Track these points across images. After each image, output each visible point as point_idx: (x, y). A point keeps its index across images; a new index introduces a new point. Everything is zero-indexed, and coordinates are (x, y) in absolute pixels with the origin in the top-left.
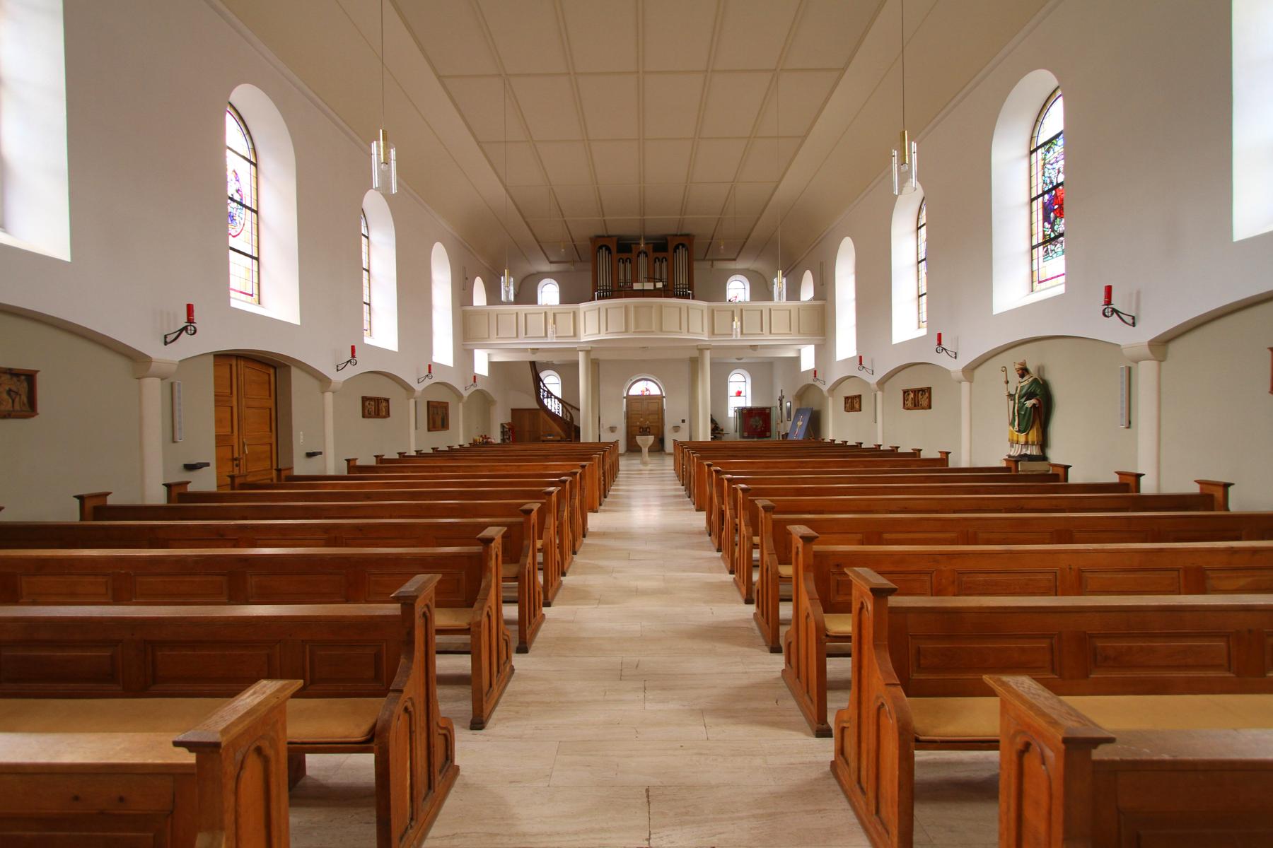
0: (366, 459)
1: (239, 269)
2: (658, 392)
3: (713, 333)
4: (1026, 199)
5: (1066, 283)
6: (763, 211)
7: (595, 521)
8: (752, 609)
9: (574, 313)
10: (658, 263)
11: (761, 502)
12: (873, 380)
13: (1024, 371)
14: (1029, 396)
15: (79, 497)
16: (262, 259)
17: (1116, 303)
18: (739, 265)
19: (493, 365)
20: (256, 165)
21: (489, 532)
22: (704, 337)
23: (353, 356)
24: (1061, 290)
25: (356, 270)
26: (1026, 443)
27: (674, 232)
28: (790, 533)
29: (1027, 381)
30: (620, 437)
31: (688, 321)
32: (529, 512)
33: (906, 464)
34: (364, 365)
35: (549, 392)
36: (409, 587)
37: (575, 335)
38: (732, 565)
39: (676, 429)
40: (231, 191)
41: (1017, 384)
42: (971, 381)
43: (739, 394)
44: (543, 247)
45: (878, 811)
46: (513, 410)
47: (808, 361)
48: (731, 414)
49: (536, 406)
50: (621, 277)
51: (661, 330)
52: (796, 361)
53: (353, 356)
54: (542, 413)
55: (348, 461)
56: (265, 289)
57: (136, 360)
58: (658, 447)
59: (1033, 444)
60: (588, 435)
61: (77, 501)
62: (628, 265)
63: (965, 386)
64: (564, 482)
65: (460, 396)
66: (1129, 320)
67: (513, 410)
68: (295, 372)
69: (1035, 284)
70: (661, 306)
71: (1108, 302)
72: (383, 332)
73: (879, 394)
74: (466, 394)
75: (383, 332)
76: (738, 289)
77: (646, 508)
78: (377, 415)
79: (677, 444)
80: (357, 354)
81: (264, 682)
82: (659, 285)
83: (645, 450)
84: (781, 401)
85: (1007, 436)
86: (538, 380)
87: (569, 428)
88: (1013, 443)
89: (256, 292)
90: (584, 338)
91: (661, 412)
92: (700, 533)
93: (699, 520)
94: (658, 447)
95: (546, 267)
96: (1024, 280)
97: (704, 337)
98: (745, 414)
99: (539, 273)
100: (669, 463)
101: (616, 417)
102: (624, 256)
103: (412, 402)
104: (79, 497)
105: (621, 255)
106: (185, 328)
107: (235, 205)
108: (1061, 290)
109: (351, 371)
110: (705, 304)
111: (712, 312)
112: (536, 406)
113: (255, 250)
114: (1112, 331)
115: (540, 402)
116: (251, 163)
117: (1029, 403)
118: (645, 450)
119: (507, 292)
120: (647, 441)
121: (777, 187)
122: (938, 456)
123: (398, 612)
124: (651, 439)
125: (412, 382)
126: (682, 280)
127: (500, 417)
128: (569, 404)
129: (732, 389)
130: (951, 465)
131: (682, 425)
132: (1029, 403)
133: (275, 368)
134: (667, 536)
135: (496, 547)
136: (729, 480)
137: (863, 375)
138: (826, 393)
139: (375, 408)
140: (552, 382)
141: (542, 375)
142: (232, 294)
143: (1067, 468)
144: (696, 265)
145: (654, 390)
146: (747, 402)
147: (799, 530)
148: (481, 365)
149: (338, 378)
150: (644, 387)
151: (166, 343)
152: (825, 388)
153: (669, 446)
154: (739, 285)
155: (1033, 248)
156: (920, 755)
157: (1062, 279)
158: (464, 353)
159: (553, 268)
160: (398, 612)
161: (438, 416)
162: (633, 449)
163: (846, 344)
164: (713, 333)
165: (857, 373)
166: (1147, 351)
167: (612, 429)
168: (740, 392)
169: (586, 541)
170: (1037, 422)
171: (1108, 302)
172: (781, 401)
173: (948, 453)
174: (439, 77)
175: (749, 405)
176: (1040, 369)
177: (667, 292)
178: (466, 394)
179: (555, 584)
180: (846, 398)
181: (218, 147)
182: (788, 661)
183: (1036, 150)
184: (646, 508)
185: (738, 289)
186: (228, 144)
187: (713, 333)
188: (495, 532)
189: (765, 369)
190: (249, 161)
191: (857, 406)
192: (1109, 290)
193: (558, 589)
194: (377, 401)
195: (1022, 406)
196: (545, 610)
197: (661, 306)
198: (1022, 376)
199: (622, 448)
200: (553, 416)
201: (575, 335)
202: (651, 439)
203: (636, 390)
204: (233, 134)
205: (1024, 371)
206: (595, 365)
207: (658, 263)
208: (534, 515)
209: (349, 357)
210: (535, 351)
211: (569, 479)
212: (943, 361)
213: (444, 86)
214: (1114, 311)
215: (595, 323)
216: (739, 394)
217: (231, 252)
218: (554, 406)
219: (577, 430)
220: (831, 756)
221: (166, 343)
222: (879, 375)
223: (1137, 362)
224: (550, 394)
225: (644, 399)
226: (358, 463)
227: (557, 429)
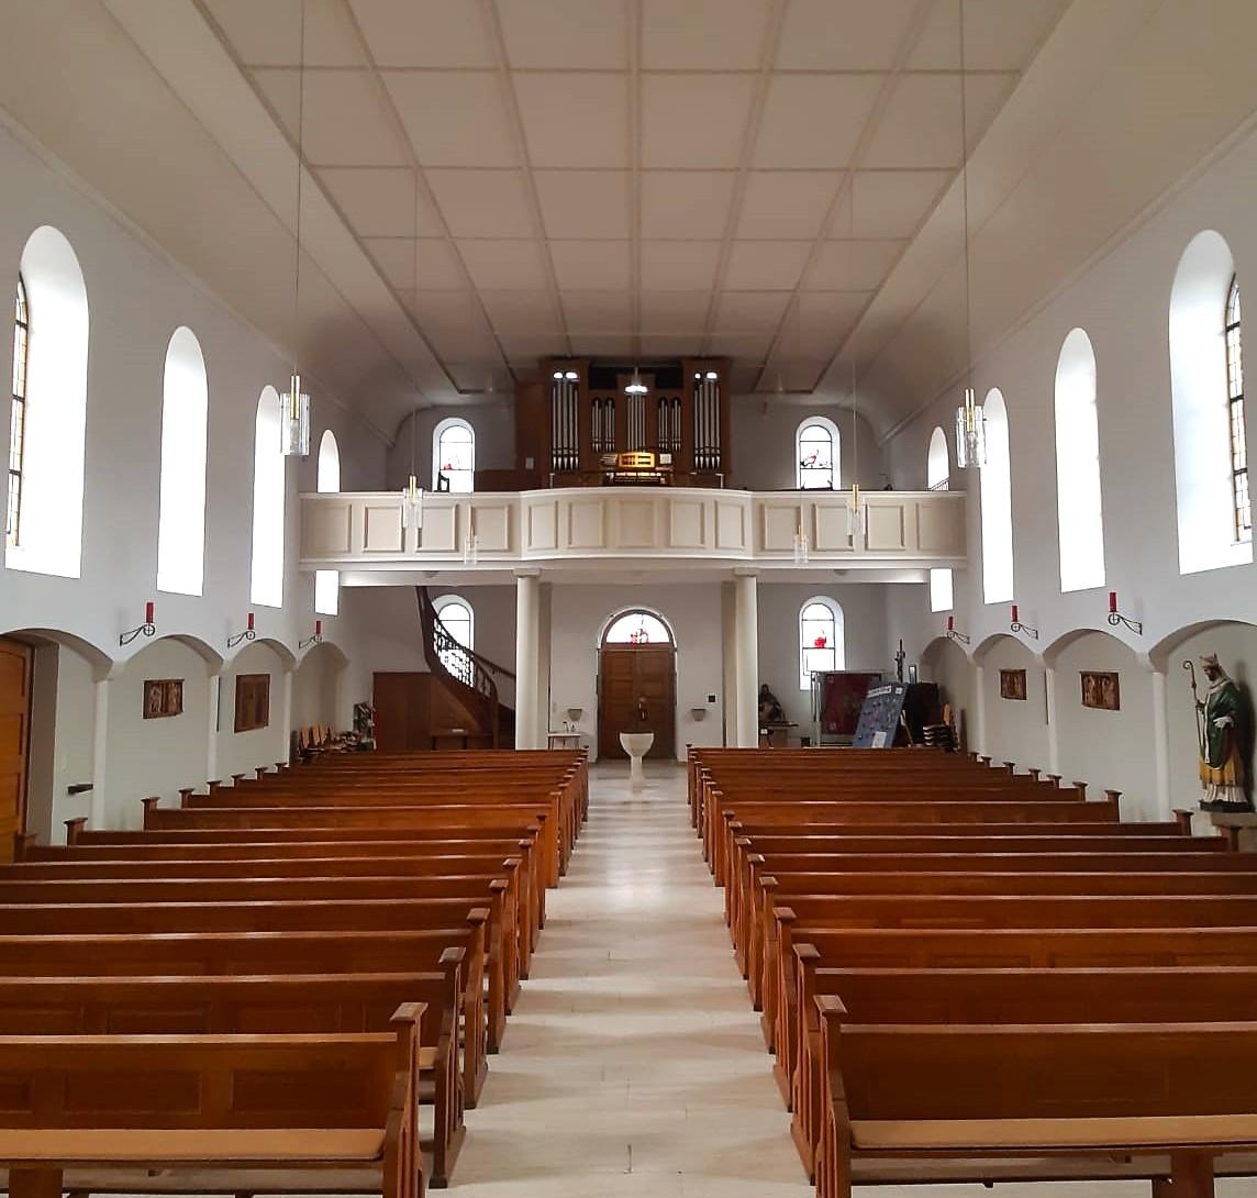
0: (170, 801)
3: (762, 548)
6: (876, 292)
9: (511, 508)
10: (664, 409)
13: (1214, 671)
14: (1219, 709)
16: (25, 473)
19: (346, 593)
22: (746, 554)
23: (149, 620)
26: (1222, 784)
29: (1220, 684)
30: (588, 728)
31: (720, 527)
33: (1052, 812)
35: (449, 638)
39: (699, 714)
41: (1208, 690)
43: (821, 643)
44: (447, 369)
46: (375, 674)
47: (942, 597)
48: (806, 683)
49: (423, 667)
50: (596, 432)
52: (923, 589)
53: (149, 620)
55: (146, 802)
58: (662, 753)
59: (1231, 786)
60: (528, 735)
62: (609, 411)
67: (375, 674)
68: (65, 655)
69: (1241, 528)
70: (667, 502)
73: (1050, 672)
74: (299, 655)
76: (818, 447)
77: (638, 877)
79: (698, 755)
82: (666, 458)
83: (636, 761)
84: (900, 661)
85: (1197, 772)
86: (429, 616)
87: (490, 714)
88: (1207, 781)
92: (717, 923)
93: (715, 901)
94: (662, 753)
95: (450, 397)
97: (747, 554)
99: (435, 407)
100: (680, 785)
101: (579, 687)
103: (215, 679)
105: (596, 393)
111: (760, 510)
112: (423, 667)
115: (432, 658)
117: (1221, 722)
118: (636, 761)
120: (634, 743)
121: (873, 298)
122: (1106, 798)
123: (443, 977)
124: (648, 739)
126: (707, 437)
127: (353, 692)
128: (492, 663)
129: (808, 634)
130: (1124, 818)
131: (710, 707)
132: (1221, 722)
133: (32, 647)
134: (672, 925)
138: (971, 660)
140: (456, 619)
141: (436, 605)
145: (656, 633)
146: (833, 660)
148: (327, 601)
150: (636, 628)
152: (969, 650)
153: (682, 755)
154: (822, 434)
155: (1236, 473)
158: (300, 583)
159: (465, 399)
160: (443, 977)
161: (251, 704)
162: (611, 753)
163: (998, 583)
164: (761, 545)
165: (1012, 634)
167: (575, 714)
168: (823, 642)
169: (543, 933)
170: (1235, 751)
172: (900, 661)
175: (841, 667)
176: (1241, 667)
177: (681, 474)
178: (299, 655)
185: (818, 447)
187: (762, 548)
189: (868, 603)
191: (1019, 689)
195: (1211, 723)
197: (667, 502)
198: (1212, 678)
199: (592, 755)
201: (511, 548)
202: (648, 739)
205: (1214, 671)
207: (664, 409)
212: (1119, 632)
215: (545, 529)
216: (821, 643)
218: (455, 664)
219: (508, 717)
224: (451, 642)
225: (633, 652)
227: (463, 712)
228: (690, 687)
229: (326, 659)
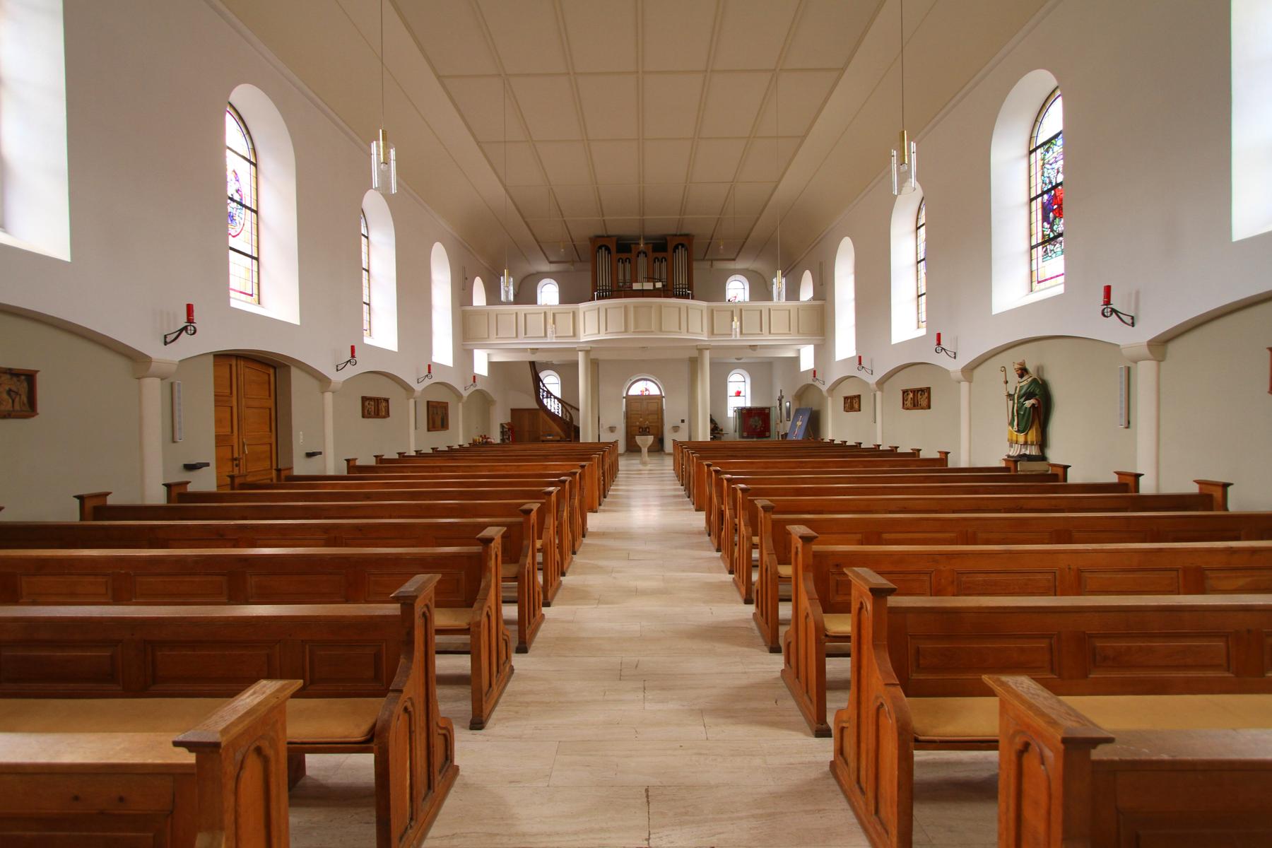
0: (366, 459)
1: (239, 269)
2: (657, 392)
3: (712, 333)
4: (1025, 199)
5: (1066, 283)
6: (762, 211)
7: (594, 521)
8: (752, 609)
9: (574, 313)
10: (657, 263)
11: (760, 502)
12: (872, 380)
13: (1023, 371)
14: (1028, 396)
15: (79, 497)
16: (262, 259)
17: (1115, 303)
18: (739, 265)
19: (492, 365)
20: (255, 165)
21: (489, 532)
22: (703, 337)
23: (353, 356)
24: (1060, 290)
25: (355, 270)
26: (1026, 443)
27: (674, 232)
28: (789, 533)
29: (1026, 381)
30: (620, 437)
31: (687, 321)
32: (528, 512)
33: (905, 464)
34: (363, 365)
35: (548, 392)
36: (409, 587)
37: (574, 335)
38: (732, 565)
39: (676, 429)
40: (231, 191)
41: (1016, 384)
42: (970, 381)
43: (738, 394)
44: (543, 247)
45: (877, 811)
46: (513, 410)
47: (807, 361)
48: (731, 414)
49: (536, 406)
50: (621, 277)
51: (661, 330)
52: (796, 361)
53: (353, 356)
54: (542, 413)
55: (348, 461)
56: (265, 289)
57: (136, 360)
58: (658, 447)
59: (1032, 444)
60: (587, 435)
61: (77, 501)
62: (628, 265)
63: (964, 386)
64: (564, 482)
65: (459, 396)
66: (1128, 320)
67: (513, 410)
68: (295, 372)
69: (1035, 284)
70: (660, 306)
71: (1107, 302)
72: (383, 332)
73: (879, 394)
74: (465, 394)
75: (383, 332)
77: (646, 508)
78: (377, 415)
79: (676, 444)
80: (356, 354)
81: (264, 682)
82: (659, 285)
83: (645, 450)
84: (780, 401)
85: (1007, 436)
86: (537, 380)
87: (569, 428)
88: (1012, 443)
89: (255, 292)
90: (583, 338)
91: (660, 412)
92: (700, 533)
93: (698, 520)
94: (658, 447)
95: (546, 267)
96: (1023, 280)
97: (704, 337)
98: (744, 414)
99: (538, 273)
100: (669, 463)
101: (615, 417)
102: (624, 256)
103: (412, 402)
104: (79, 497)
105: (620, 255)
106: (185, 328)
107: (235, 205)
108: (1060, 290)
109: (351, 371)
110: (704, 304)
111: (712, 312)
112: (536, 406)
113: (255, 250)
114: (1111, 331)
115: (540, 402)
116: (251, 163)
117: (1028, 403)
118: (645, 450)
119: (507, 292)
120: (646, 441)
121: (776, 187)
122: (938, 456)
123: (398, 612)
124: (650, 439)
125: (411, 382)
126: (681, 280)
127: (500, 417)
128: (569, 404)
129: (732, 389)
130: (950, 465)
131: (682, 425)
132: (1028, 403)
133: (275, 368)
134: (666, 536)
135: (496, 547)
136: (728, 480)
137: (863, 375)
138: (825, 393)
139: (375, 408)
140: (552, 382)
141: (542, 375)
142: (232, 294)
143: (1066, 468)
144: (695, 265)
145: (654, 390)
146: (746, 402)
147: (798, 530)
148: (481, 365)
149: (337, 378)
150: (643, 387)
151: (166, 343)
152: (824, 388)
153: (669, 446)
154: (739, 285)
155: (1032, 248)
156: (919, 755)
157: (1062, 279)
158: (464, 353)
159: (553, 268)
160: (398, 612)
161: (437, 416)
162: (633, 449)
163: (845, 344)
164: (712, 333)
165: (857, 373)
166: (1146, 351)
167: (612, 429)
168: (740, 392)
169: (586, 541)
170: (1037, 422)
171: (1107, 302)
172: (780, 401)
173: (947, 453)
174: (439, 77)
175: (748, 405)
176: (1040, 369)
177: (667, 292)
178: (465, 394)
179: (555, 584)
180: (846, 398)
181: (218, 147)
182: (788, 661)
183: (1035, 150)
184: (646, 508)
185: (737, 289)
186: (228, 144)
187: (712, 333)
188: (495, 532)
189: (764, 369)
190: (249, 161)
191: (856, 406)
192: (1108, 290)
193: (557, 589)
194: (377, 401)
195: (1021, 406)
196: (544, 610)
197: (660, 306)
198: (1021, 376)
199: (621, 448)
200: (552, 416)
201: (574, 335)
202: (650, 439)
203: (636, 390)
204: (233, 134)
205: (1023, 371)
206: (594, 365)
207: (657, 263)
208: (533, 515)
209: (349, 357)
210: (534, 351)
211: (569, 479)
213: (444, 86)
214: (1113, 311)
215: (594, 323)
216: (738, 394)
217: (231, 252)
218: (553, 406)
219: (577, 430)
220: (830, 756)
221: (166, 343)
222: (878, 375)
223: (1136, 362)
224: (549, 394)
225: (644, 399)
226: (358, 463)
227: (557, 429)
228: (673, 413)
229: (482, 400)
